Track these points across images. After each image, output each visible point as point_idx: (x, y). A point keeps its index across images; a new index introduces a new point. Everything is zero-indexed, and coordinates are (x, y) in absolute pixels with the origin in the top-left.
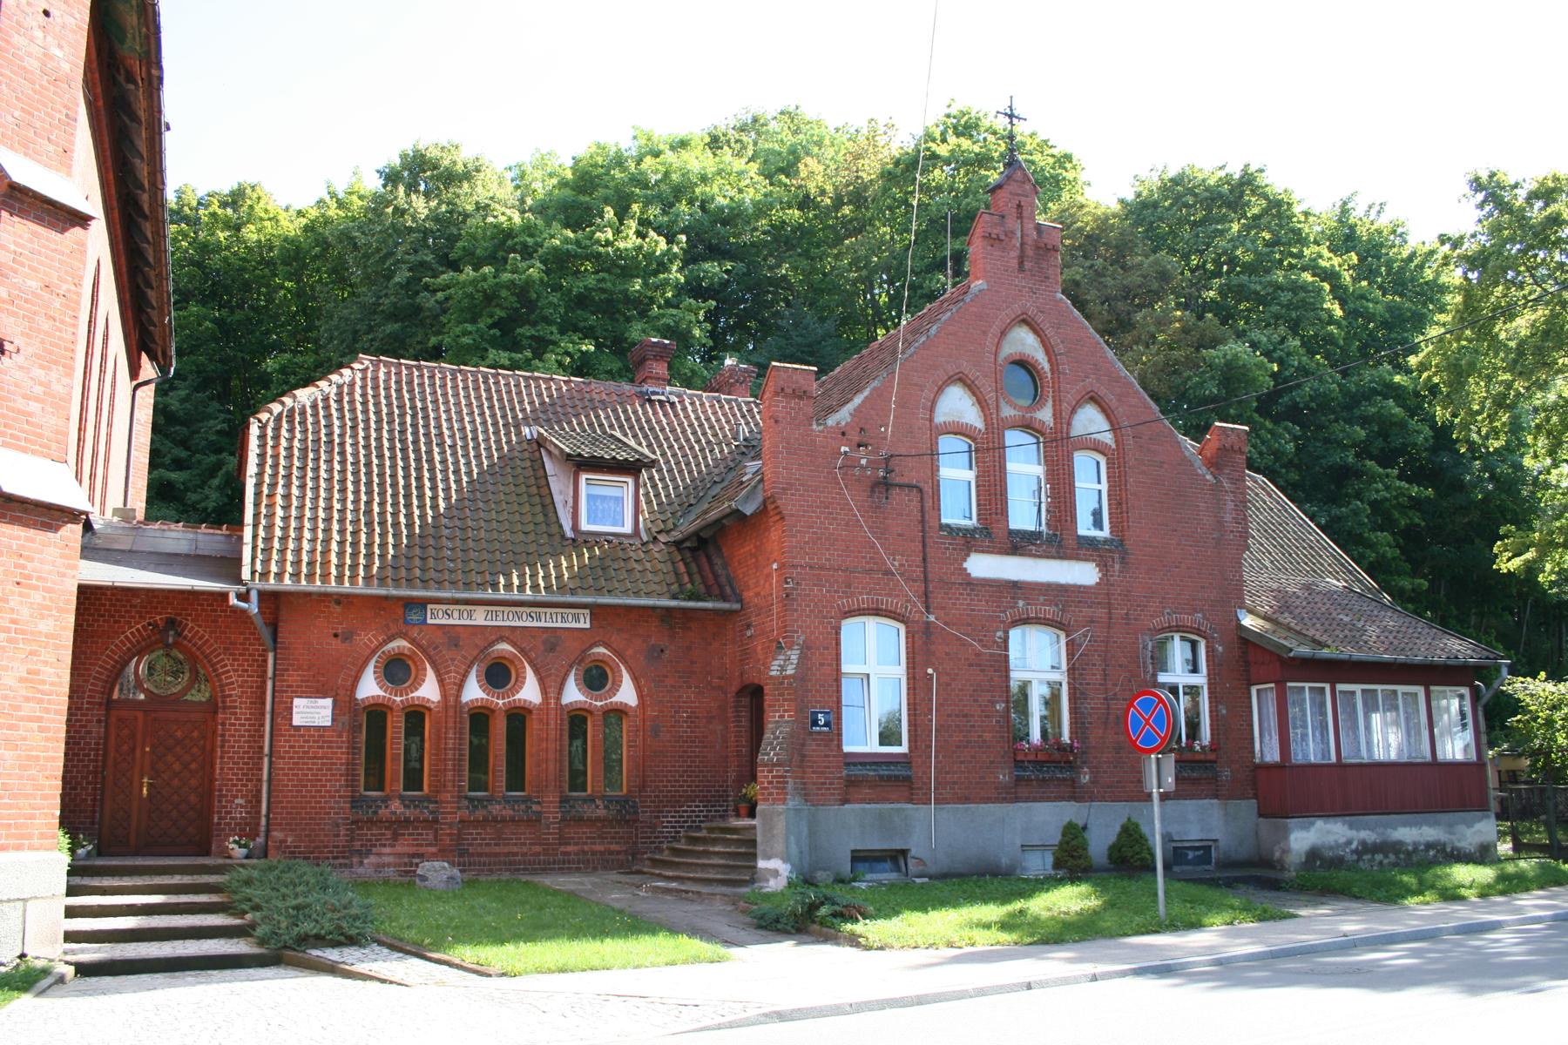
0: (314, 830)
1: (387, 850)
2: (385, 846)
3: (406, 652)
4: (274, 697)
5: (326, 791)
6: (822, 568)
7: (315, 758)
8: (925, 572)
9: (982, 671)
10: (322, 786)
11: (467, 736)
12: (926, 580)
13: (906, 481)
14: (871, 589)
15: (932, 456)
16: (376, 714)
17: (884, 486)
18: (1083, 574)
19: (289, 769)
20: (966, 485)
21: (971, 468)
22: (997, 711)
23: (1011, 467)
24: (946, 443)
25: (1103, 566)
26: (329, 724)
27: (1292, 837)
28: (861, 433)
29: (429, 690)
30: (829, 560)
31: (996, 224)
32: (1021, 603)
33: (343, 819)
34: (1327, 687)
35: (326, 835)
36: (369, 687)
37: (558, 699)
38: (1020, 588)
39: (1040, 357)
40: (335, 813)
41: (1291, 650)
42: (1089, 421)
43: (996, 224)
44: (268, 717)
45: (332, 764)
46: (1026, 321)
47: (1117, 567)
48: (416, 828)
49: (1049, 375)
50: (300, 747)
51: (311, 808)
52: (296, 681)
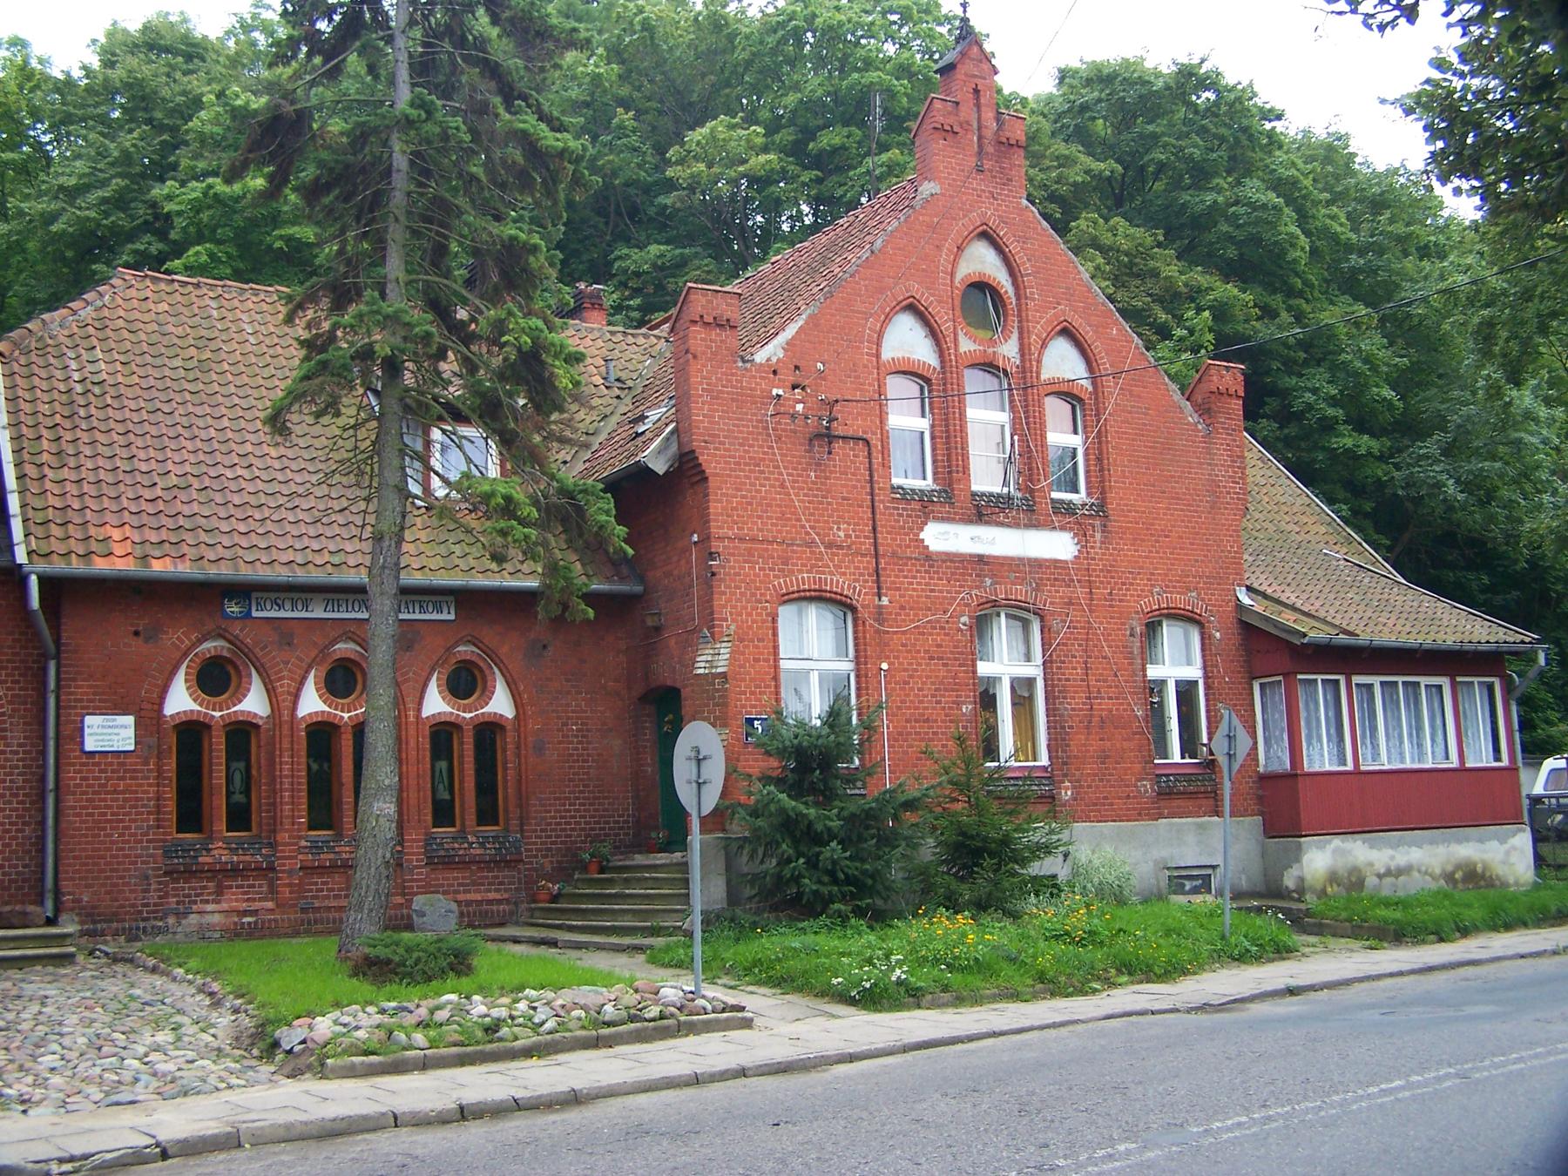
0: (116, 885)
1: (210, 907)
2: (207, 902)
3: (225, 654)
4: (58, 716)
5: (131, 835)
6: (754, 540)
7: (115, 792)
8: (876, 545)
9: (945, 665)
10: (125, 828)
11: (304, 760)
12: (876, 555)
13: (850, 433)
14: (813, 566)
15: (879, 403)
16: (191, 732)
17: (826, 437)
18: (1057, 545)
19: (82, 808)
20: (918, 435)
21: (923, 416)
22: (964, 715)
23: (971, 413)
24: (898, 387)
25: (1082, 535)
26: (132, 748)
27: (1306, 859)
28: (795, 371)
29: (254, 703)
30: (761, 530)
31: (950, 113)
32: (988, 581)
33: (154, 869)
34: (1342, 679)
35: (131, 891)
36: (180, 700)
37: (419, 710)
38: (987, 563)
39: (1002, 278)
40: (142, 863)
41: (1305, 635)
42: (1061, 362)
43: (950, 113)
44: (51, 743)
45: (137, 799)
46: (987, 236)
47: (1098, 536)
48: (247, 878)
49: (1014, 300)
50: (95, 778)
51: (112, 856)
52: (86, 694)
